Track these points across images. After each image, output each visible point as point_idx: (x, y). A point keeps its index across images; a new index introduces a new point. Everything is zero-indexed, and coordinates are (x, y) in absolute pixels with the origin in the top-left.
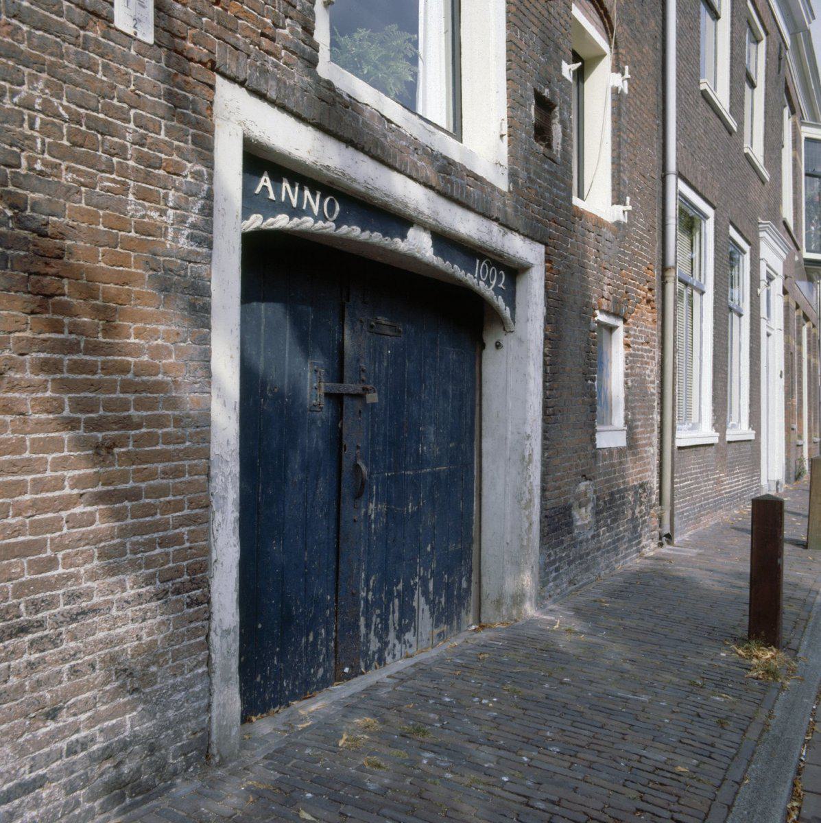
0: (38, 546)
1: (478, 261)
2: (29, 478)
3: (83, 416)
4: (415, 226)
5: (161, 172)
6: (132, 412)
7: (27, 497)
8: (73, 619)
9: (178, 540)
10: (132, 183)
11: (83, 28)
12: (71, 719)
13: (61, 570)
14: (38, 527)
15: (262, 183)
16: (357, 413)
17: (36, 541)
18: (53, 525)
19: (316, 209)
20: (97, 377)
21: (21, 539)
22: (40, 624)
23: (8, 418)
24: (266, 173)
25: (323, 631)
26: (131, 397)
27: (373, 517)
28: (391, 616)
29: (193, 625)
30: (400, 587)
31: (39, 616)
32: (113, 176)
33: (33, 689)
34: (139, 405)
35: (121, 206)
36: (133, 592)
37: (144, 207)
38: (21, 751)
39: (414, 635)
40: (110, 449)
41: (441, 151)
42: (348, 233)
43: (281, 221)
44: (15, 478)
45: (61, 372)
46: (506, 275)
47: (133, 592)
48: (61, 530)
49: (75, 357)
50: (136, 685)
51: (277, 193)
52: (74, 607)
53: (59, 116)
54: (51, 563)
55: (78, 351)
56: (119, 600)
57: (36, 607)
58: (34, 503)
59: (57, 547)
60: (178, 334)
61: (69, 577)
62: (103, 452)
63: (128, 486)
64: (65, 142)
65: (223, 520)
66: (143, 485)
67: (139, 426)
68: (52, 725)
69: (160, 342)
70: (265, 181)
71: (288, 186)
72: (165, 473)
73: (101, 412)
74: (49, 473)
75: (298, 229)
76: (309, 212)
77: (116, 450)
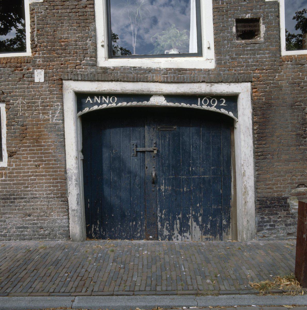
0: (25, 184)
1: (199, 99)
2: (22, 171)
3: (32, 159)
4: (153, 96)
5: (48, 107)
6: (43, 158)
7: (22, 174)
8: (32, 198)
9: (57, 186)
10: (41, 112)
11: (29, 85)
12: (33, 218)
13: (29, 189)
14: (24, 180)
15: (88, 99)
16: (153, 157)
17: (24, 183)
18: (27, 180)
19: (107, 102)
20: (35, 152)
21: (21, 182)
22: (26, 198)
23: (18, 160)
24: (89, 97)
25: (140, 222)
26: (43, 155)
27: (163, 190)
28: (175, 225)
29: (62, 206)
30: (180, 216)
31: (25, 196)
32: (37, 111)
33: (25, 210)
34: (45, 157)
35: (38, 117)
36: (46, 196)
37: (44, 116)
38: (23, 221)
39: (190, 235)
40: (39, 166)
41: (164, 67)
42: (121, 105)
43: (96, 107)
44: (19, 171)
45: (27, 151)
46: (217, 101)
47: (46, 196)
48: (29, 181)
49: (30, 148)
50: (48, 216)
51: (93, 101)
52: (32, 196)
53: (24, 104)
54: (27, 187)
55: (31, 147)
56: (43, 197)
57: (24, 195)
58: (23, 176)
59: (28, 184)
60: (54, 141)
61: (31, 190)
62: (38, 166)
63: (43, 174)
64: (26, 108)
65: (71, 183)
66: (47, 174)
67: (45, 161)
68: (28, 218)
69: (50, 143)
70: (89, 99)
71: (97, 98)
72: (52, 172)
73: (36, 158)
74: (26, 170)
75: (102, 108)
76: (105, 102)
77: (40, 166)
